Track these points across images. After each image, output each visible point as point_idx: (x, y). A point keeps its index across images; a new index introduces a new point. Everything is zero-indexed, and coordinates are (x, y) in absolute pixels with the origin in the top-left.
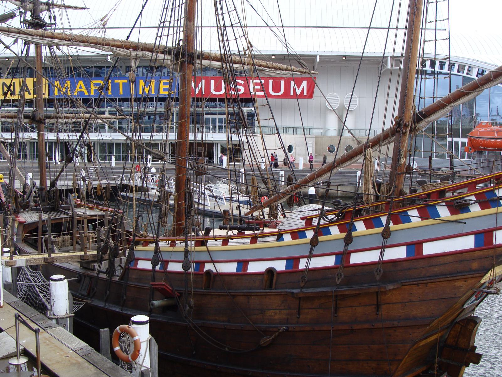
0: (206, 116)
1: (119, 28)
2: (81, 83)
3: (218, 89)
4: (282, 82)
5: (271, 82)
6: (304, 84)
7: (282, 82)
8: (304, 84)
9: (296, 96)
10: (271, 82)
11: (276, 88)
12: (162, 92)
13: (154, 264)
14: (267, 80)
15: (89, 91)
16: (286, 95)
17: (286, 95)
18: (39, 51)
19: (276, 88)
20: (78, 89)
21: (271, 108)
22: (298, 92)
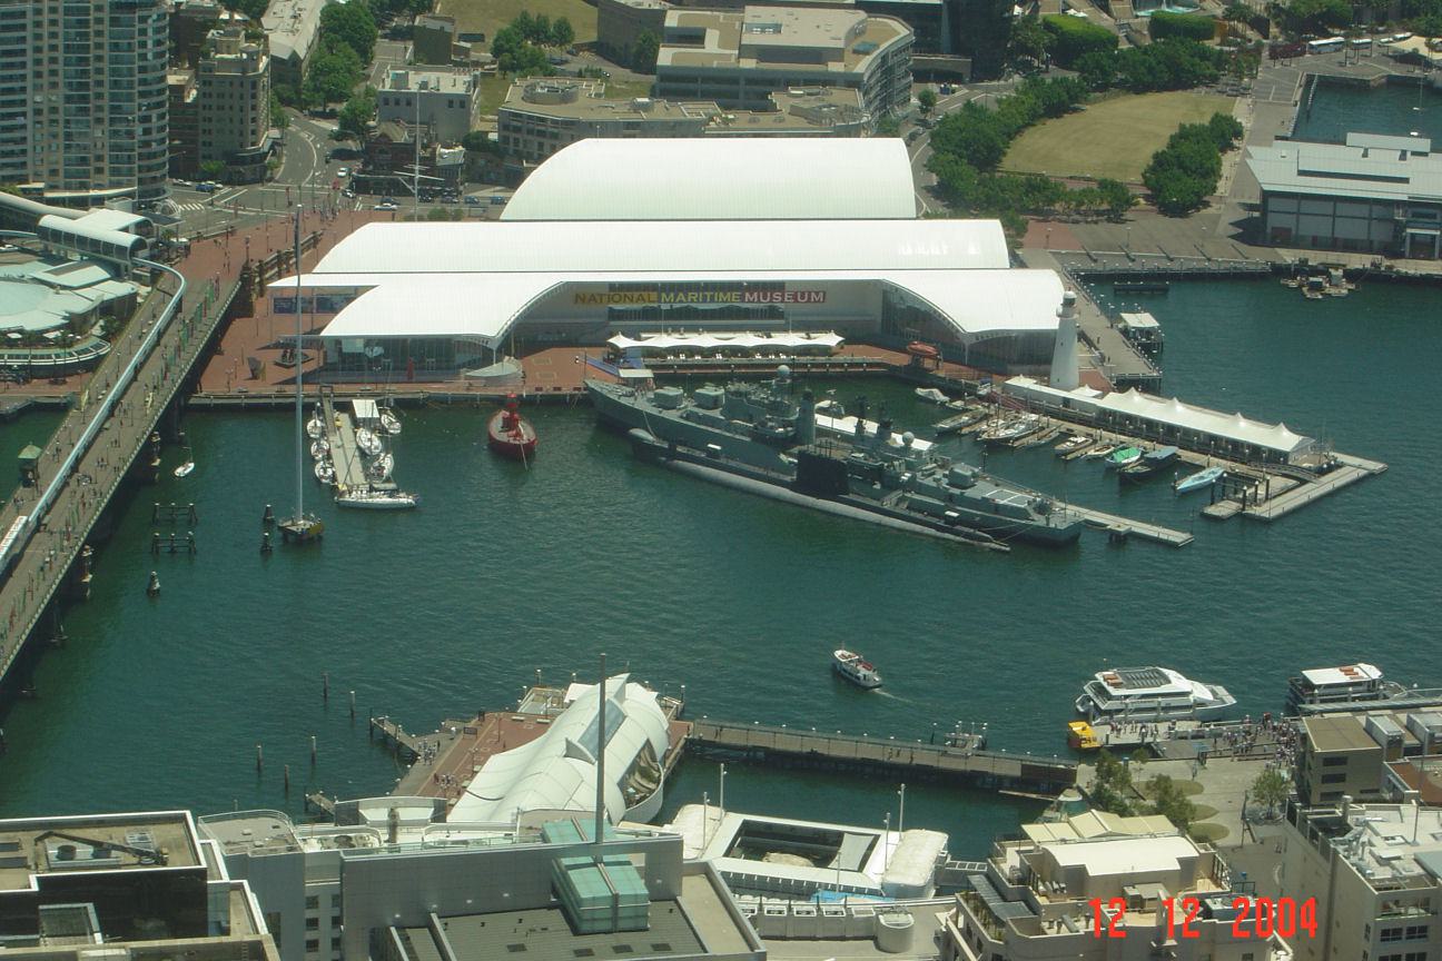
9: (815, 301)
11: (803, 297)
19: (803, 297)
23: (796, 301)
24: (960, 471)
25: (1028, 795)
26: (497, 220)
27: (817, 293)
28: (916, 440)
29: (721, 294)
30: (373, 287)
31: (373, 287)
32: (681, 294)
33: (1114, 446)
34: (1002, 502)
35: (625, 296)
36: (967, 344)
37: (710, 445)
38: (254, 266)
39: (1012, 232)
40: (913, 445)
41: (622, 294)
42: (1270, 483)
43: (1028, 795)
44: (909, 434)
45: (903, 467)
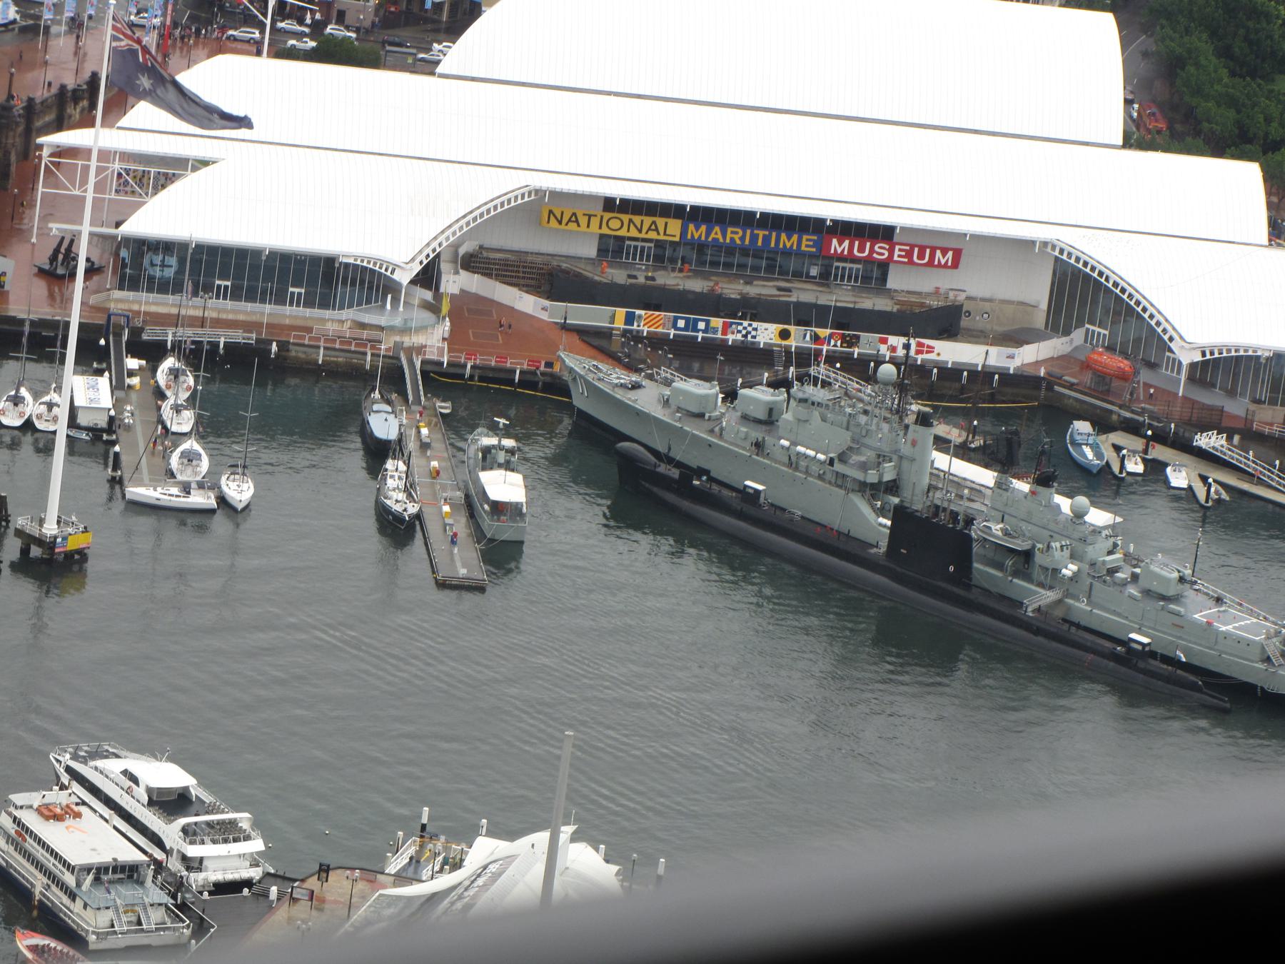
0: (836, 264)
1: (1087, 144)
2: (717, 229)
3: (861, 250)
4: (928, 251)
5: (916, 250)
6: (950, 254)
7: (928, 251)
8: (950, 254)
9: (939, 265)
10: (916, 250)
11: (921, 256)
12: (803, 248)
13: (546, 287)
14: (912, 247)
15: (724, 238)
16: (930, 263)
17: (930, 263)
18: (246, 46)
19: (921, 256)
20: (713, 235)
21: (55, 246)
22: (943, 262)
23: (911, 262)
24: (1157, 570)
25: (655, 489)
26: (432, 73)
27: (922, 250)
28: (1093, 511)
29: (783, 236)
30: (205, 163)
31: (205, 163)
32: (717, 229)
33: (862, 369)
34: (1223, 628)
35: (631, 221)
36: (1185, 361)
37: (748, 483)
38: (19, 106)
39: (1275, 199)
40: (1087, 518)
41: (626, 218)
42: (15, 78)
43: (655, 489)
44: (1082, 500)
45: (1067, 553)
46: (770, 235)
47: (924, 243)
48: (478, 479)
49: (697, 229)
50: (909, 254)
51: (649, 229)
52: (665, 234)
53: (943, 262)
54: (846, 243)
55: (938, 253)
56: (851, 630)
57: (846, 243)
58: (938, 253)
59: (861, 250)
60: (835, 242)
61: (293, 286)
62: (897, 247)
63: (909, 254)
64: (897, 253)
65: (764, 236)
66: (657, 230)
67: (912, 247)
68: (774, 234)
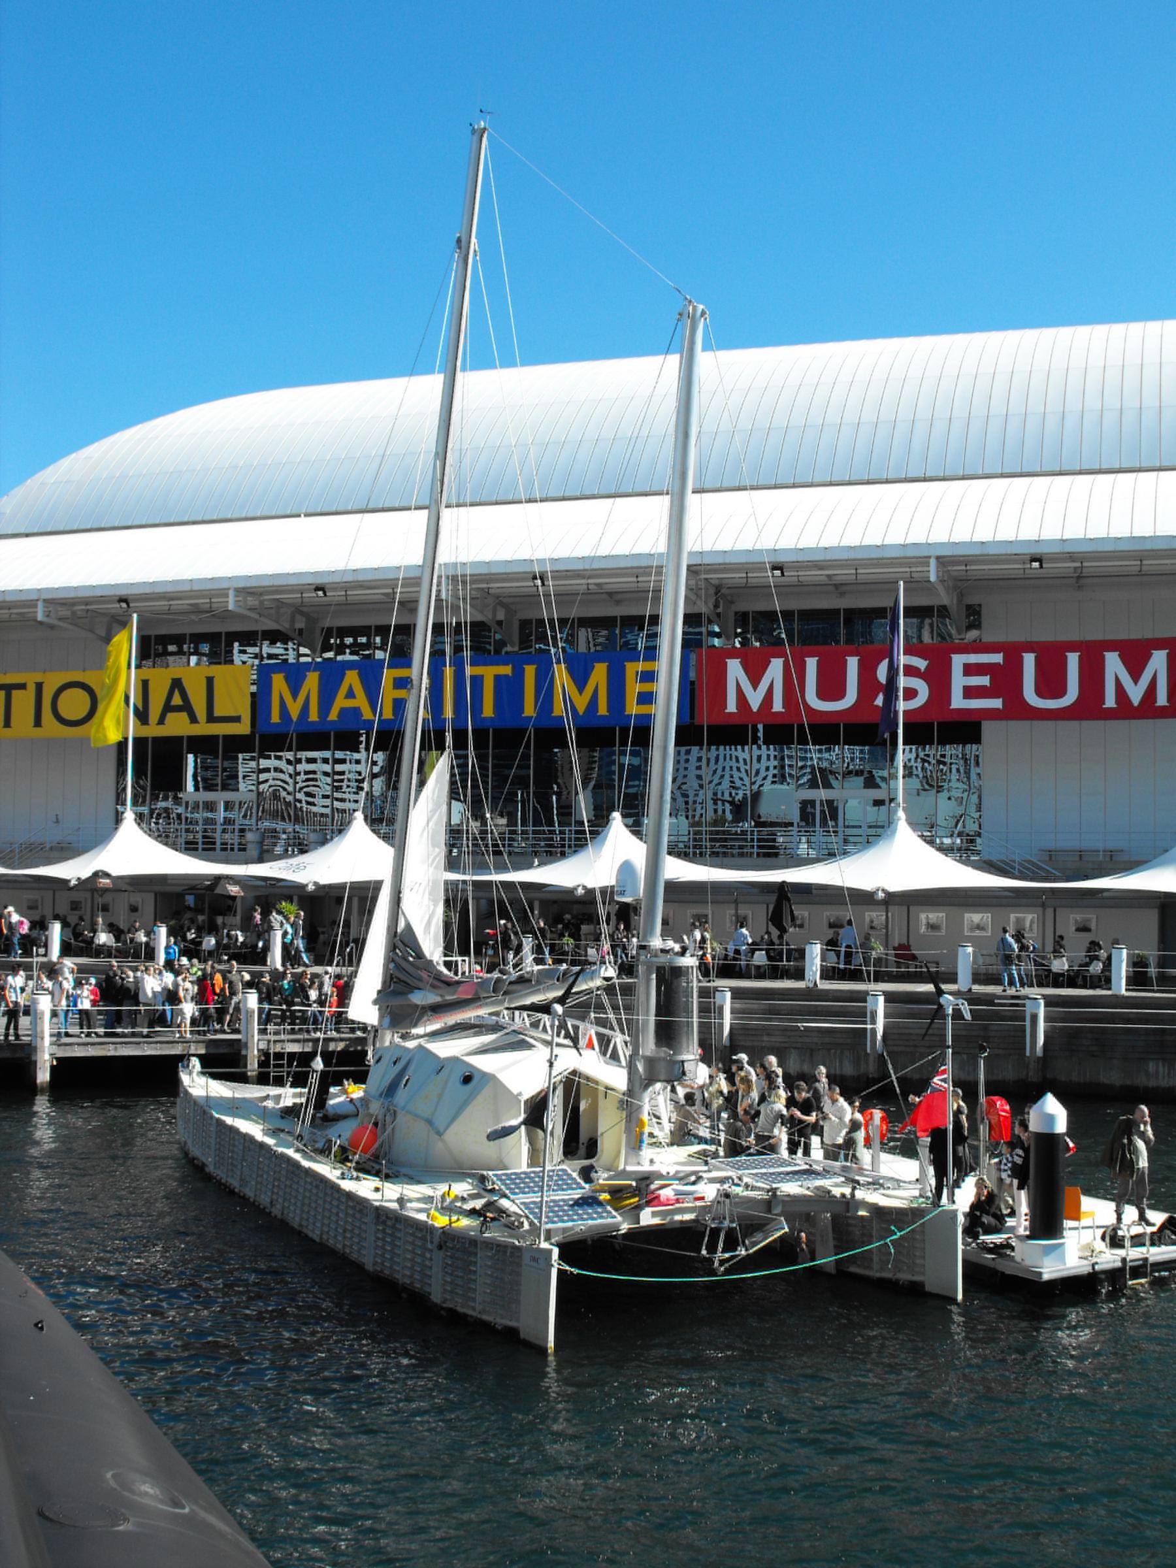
3: (831, 687)
4: (1073, 659)
5: (1029, 660)
6: (1158, 661)
7: (1073, 659)
10: (1029, 660)
11: (1051, 684)
12: (958, 701)
14: (1013, 653)
16: (1089, 706)
17: (1089, 706)
19: (1051, 684)
22: (1136, 694)
23: (1017, 710)
32: (755, 705)
46: (519, 674)
47: (1093, 633)
48: (604, 662)
49: (755, 674)
50: (1005, 680)
51: (168, 708)
52: (211, 718)
53: (1136, 694)
54: (776, 669)
55: (1113, 664)
56: (885, 1479)
57: (776, 669)
58: (1113, 664)
59: (831, 687)
60: (735, 669)
61: (1131, 1279)
62: (958, 661)
63: (1005, 680)
64: (959, 681)
65: (498, 678)
66: (187, 707)
67: (1013, 653)
68: (530, 671)
